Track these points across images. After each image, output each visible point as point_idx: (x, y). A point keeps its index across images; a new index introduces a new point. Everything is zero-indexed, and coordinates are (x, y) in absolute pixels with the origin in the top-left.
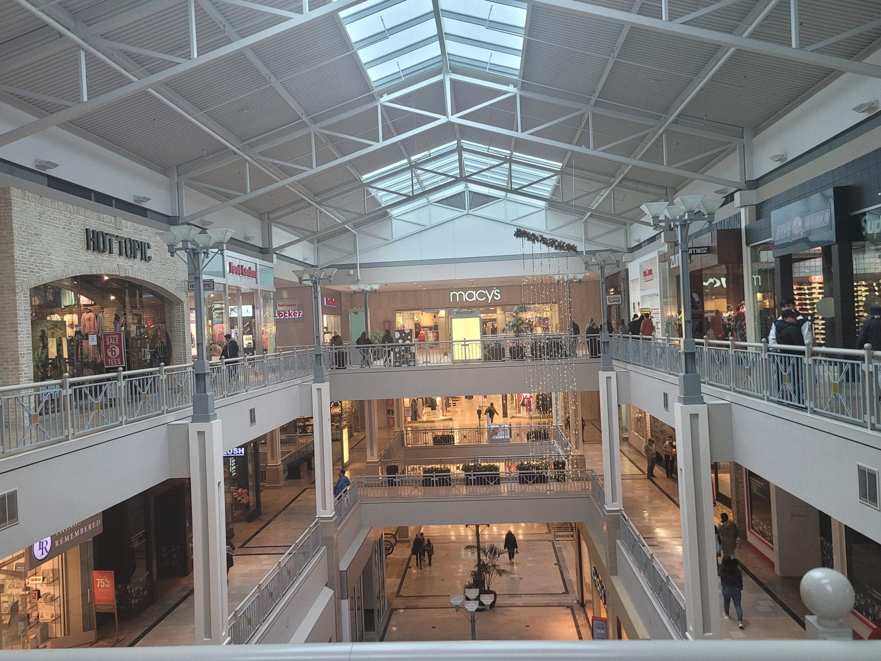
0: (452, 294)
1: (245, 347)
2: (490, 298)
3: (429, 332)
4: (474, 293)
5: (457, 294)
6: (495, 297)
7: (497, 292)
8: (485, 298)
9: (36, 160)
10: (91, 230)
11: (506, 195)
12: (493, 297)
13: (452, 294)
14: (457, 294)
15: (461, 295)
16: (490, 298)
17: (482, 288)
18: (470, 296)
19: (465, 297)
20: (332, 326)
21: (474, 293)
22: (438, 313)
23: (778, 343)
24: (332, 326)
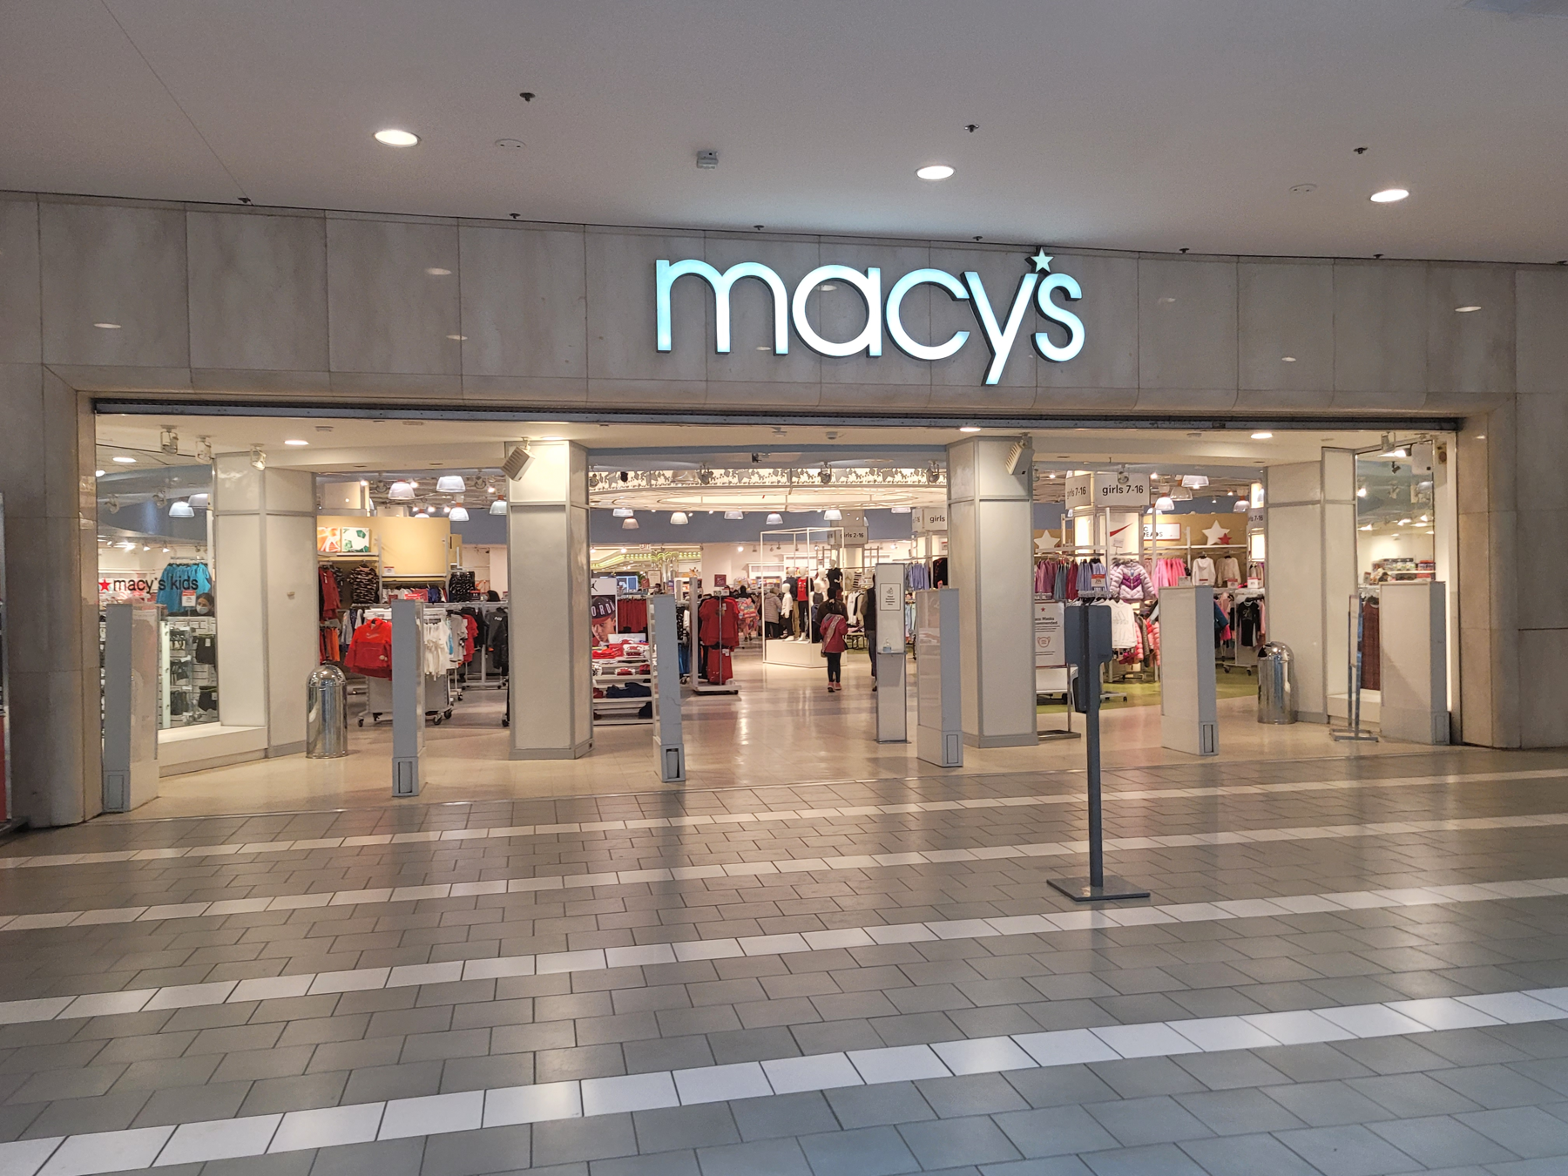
1: (924, 480)
2: (1002, 344)
3: (429, 612)
5: (722, 284)
6: (1043, 341)
7: (1061, 295)
8: (958, 341)
9: (1149, 900)
10: (819, 646)
12: (1027, 339)
13: (667, 274)
14: (722, 284)
15: (751, 293)
16: (1002, 344)
17: (931, 248)
21: (870, 284)
22: (515, 463)
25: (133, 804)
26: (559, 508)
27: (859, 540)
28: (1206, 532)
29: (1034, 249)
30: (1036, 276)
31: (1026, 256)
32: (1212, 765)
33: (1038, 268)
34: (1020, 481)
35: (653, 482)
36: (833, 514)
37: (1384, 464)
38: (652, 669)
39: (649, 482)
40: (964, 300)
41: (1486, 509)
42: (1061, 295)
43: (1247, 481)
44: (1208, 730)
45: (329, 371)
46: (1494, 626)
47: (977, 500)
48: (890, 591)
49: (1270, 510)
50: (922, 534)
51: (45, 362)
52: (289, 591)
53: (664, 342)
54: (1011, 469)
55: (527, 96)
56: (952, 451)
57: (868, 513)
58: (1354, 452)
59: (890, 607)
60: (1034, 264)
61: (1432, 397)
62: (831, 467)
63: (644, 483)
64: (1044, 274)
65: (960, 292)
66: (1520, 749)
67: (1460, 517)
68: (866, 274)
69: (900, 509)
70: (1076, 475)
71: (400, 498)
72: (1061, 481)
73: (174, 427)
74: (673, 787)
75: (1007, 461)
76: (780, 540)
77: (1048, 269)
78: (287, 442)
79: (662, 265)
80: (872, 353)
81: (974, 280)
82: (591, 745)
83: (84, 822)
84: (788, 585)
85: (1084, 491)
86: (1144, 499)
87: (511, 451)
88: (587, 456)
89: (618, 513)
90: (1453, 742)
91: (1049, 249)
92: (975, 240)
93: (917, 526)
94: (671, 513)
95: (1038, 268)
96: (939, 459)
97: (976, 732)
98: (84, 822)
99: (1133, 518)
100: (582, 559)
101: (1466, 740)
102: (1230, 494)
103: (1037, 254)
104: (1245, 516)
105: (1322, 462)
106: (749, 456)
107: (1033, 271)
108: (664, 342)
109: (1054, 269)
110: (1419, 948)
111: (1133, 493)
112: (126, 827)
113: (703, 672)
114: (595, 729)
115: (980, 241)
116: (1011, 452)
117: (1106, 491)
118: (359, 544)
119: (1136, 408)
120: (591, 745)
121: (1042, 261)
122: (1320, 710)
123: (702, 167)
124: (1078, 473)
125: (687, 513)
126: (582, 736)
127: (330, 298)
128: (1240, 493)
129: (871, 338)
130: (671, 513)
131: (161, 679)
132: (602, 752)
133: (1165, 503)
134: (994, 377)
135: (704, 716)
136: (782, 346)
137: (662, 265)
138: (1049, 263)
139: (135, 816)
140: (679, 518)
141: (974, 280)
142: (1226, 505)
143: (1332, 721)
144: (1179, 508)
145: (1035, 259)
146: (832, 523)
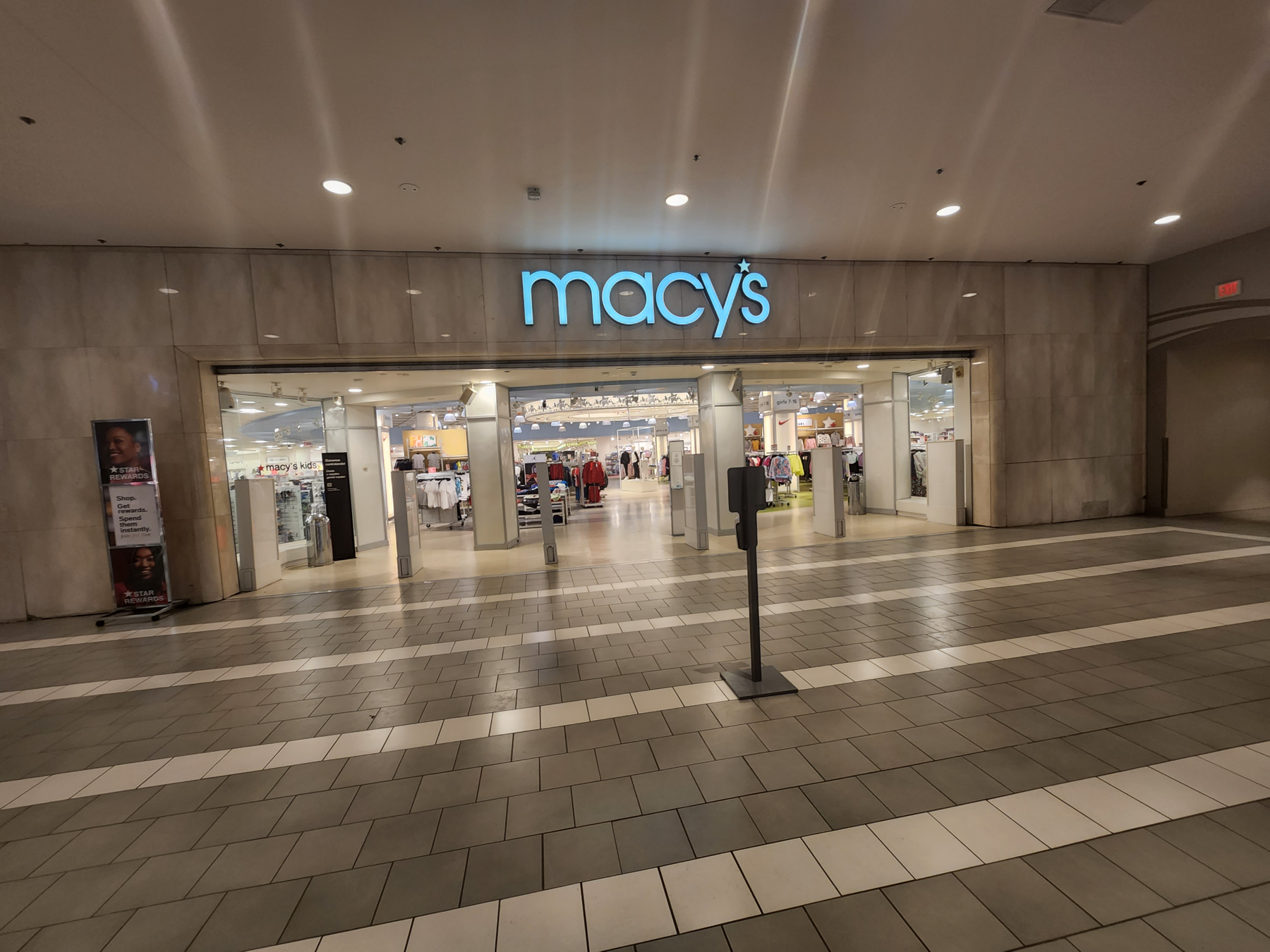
0: (529, 279)
2: (723, 313)
4: (646, 281)
7: (755, 286)
11: (390, 519)
12: (736, 313)
13: (529, 279)
14: (561, 284)
16: (723, 313)
18: (629, 296)
19: (601, 298)
20: (581, 618)
21: (646, 281)
22: (466, 396)
23: (145, 421)
24: (581, 618)
25: (258, 586)
26: (493, 419)
27: (665, 433)
28: (824, 422)
29: (739, 260)
31: (735, 264)
32: (842, 544)
33: (742, 270)
34: (736, 395)
35: (563, 408)
36: (652, 421)
37: (919, 382)
39: (561, 408)
40: (701, 290)
41: (988, 399)
42: (755, 286)
43: (841, 398)
44: (840, 524)
45: (338, 344)
46: (992, 463)
47: (713, 406)
49: (865, 407)
50: (692, 428)
51: (176, 345)
52: (365, 467)
53: (529, 319)
54: (731, 389)
55: (400, 140)
56: (700, 381)
57: (668, 419)
58: (908, 375)
59: (677, 464)
60: (740, 268)
61: (960, 339)
62: (638, 394)
63: (559, 408)
64: (745, 273)
65: (698, 285)
66: (1006, 527)
67: (972, 404)
69: (682, 417)
71: (449, 421)
72: (756, 401)
73: (305, 389)
74: (551, 568)
75: (728, 383)
76: (629, 434)
77: (748, 271)
78: (350, 390)
79: (525, 275)
81: (705, 277)
82: (518, 541)
83: (223, 599)
85: (768, 403)
86: (796, 406)
87: (465, 388)
88: (508, 392)
89: (554, 424)
90: (967, 524)
91: (748, 259)
92: (705, 255)
93: (690, 425)
94: (579, 423)
95: (742, 270)
96: (695, 385)
97: (716, 528)
98: (223, 599)
99: (792, 415)
101: (975, 523)
102: (834, 405)
103: (741, 262)
104: (842, 415)
105: (892, 380)
106: (593, 388)
107: (739, 272)
108: (529, 319)
109: (751, 270)
111: (792, 403)
112: (256, 600)
113: (587, 496)
114: (520, 530)
115: (709, 255)
116: (730, 379)
117: (779, 403)
118: (431, 443)
119: (799, 349)
120: (518, 541)
121: (744, 266)
122: (893, 508)
123: (531, 199)
124: (766, 393)
125: (587, 423)
126: (512, 535)
127: (336, 301)
128: (839, 404)
130: (579, 423)
131: (764, 445)
132: (524, 544)
133: (804, 409)
134: (719, 334)
135: (591, 521)
136: (597, 319)
137: (525, 275)
138: (749, 267)
139: (258, 594)
140: (583, 426)
141: (705, 277)
142: (832, 409)
143: (899, 513)
144: (811, 412)
145: (740, 265)
146: (652, 425)
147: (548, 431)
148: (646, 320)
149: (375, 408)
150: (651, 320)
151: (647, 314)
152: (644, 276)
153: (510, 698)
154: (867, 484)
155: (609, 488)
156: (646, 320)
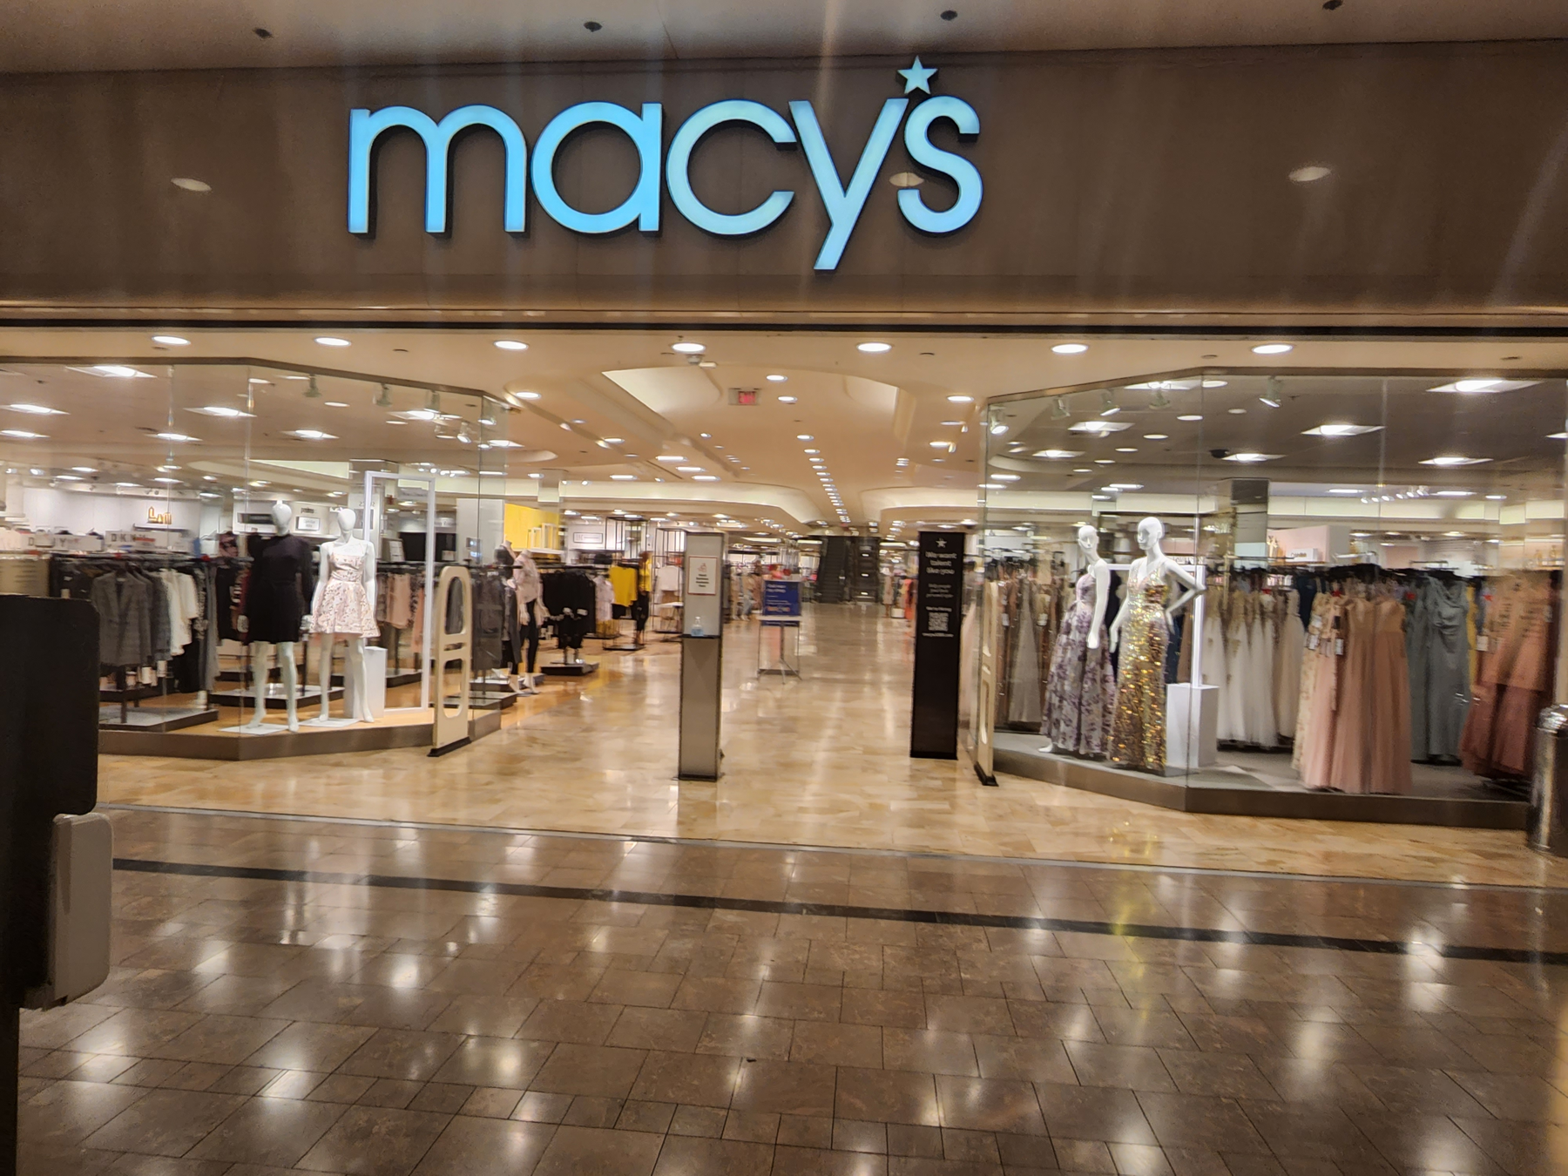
0: (365, 127)
4: (644, 128)
5: (437, 137)
7: (941, 131)
12: (881, 196)
13: (365, 127)
14: (437, 137)
16: (844, 207)
21: (644, 128)
30: (905, 101)
33: (910, 87)
38: (468, 693)
42: (941, 131)
48: (703, 567)
64: (917, 98)
65: (779, 131)
68: (639, 114)
70: (1204, 386)
80: (644, 227)
84: (972, 598)
95: (910, 87)
100: (724, 558)
109: (937, 87)
110: (123, 607)
121: (917, 77)
129: (642, 208)
136: (515, 219)
138: (930, 81)
141: (805, 116)
147: (412, 565)
148: (636, 222)
149: (333, 659)
150: (650, 223)
151: (642, 208)
152: (639, 114)
153: (1158, 966)
154: (1136, 923)
155: (422, 651)
156: (636, 222)
